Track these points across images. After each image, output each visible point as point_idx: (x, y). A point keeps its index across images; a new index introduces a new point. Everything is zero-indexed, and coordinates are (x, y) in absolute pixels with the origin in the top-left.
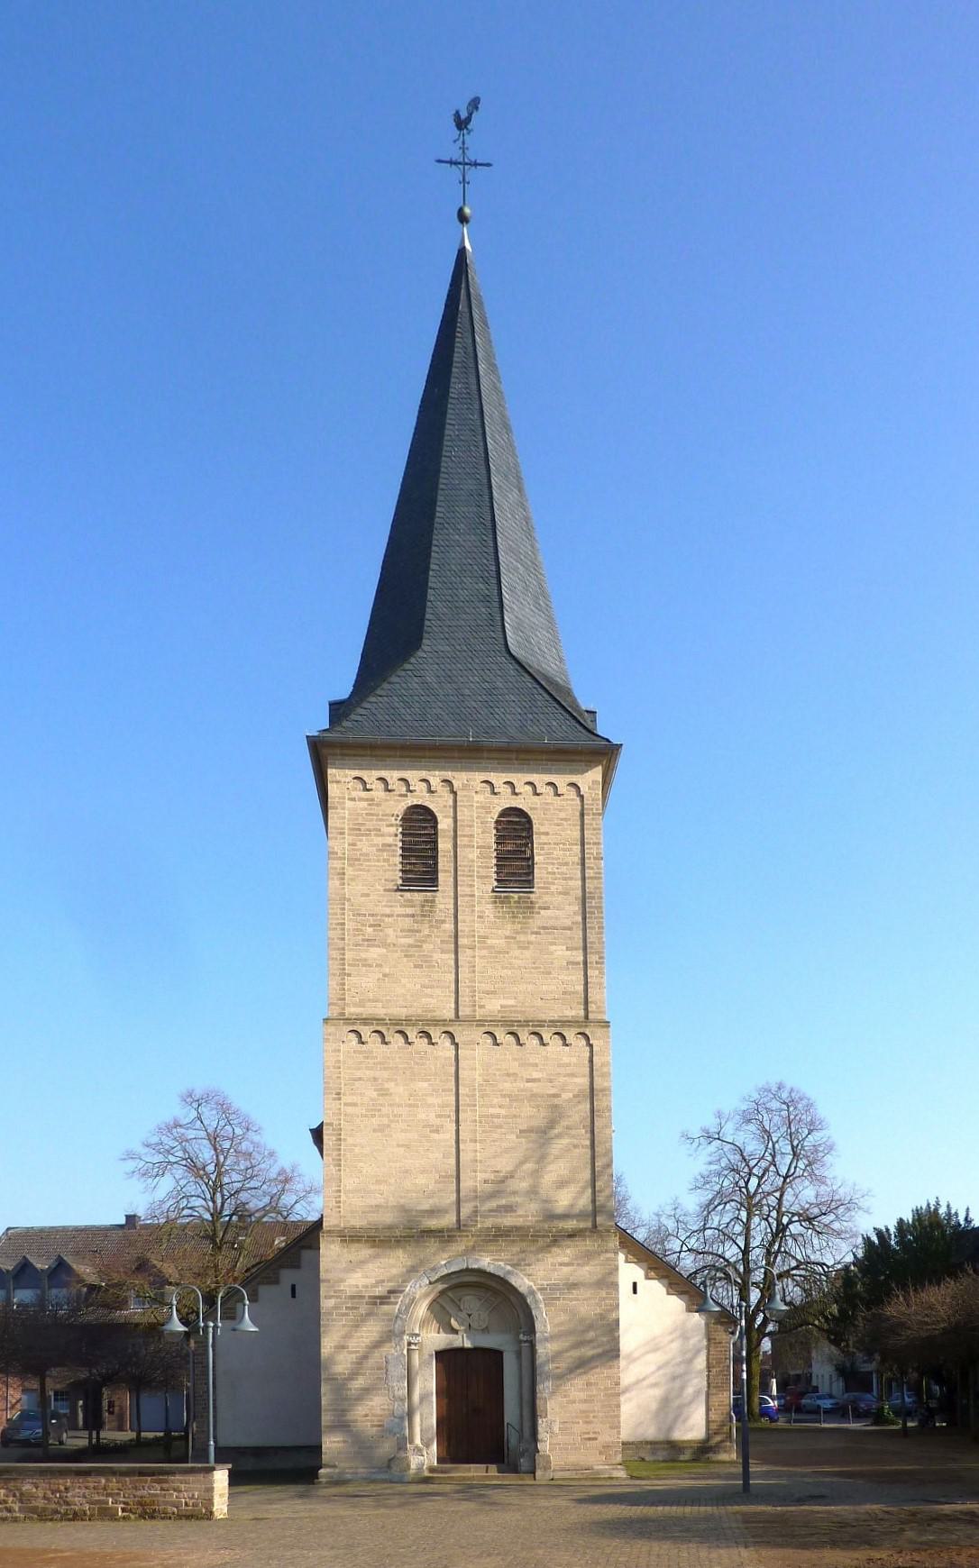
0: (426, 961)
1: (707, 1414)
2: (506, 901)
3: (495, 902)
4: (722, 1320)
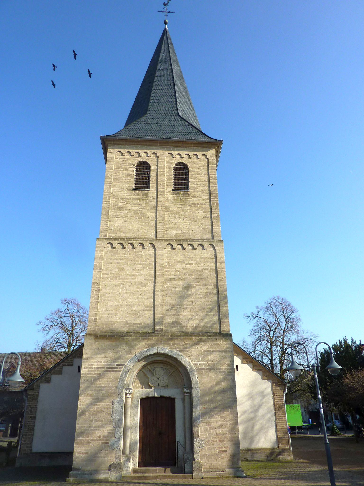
0: (144, 216)
1: (277, 434)
4: (279, 384)
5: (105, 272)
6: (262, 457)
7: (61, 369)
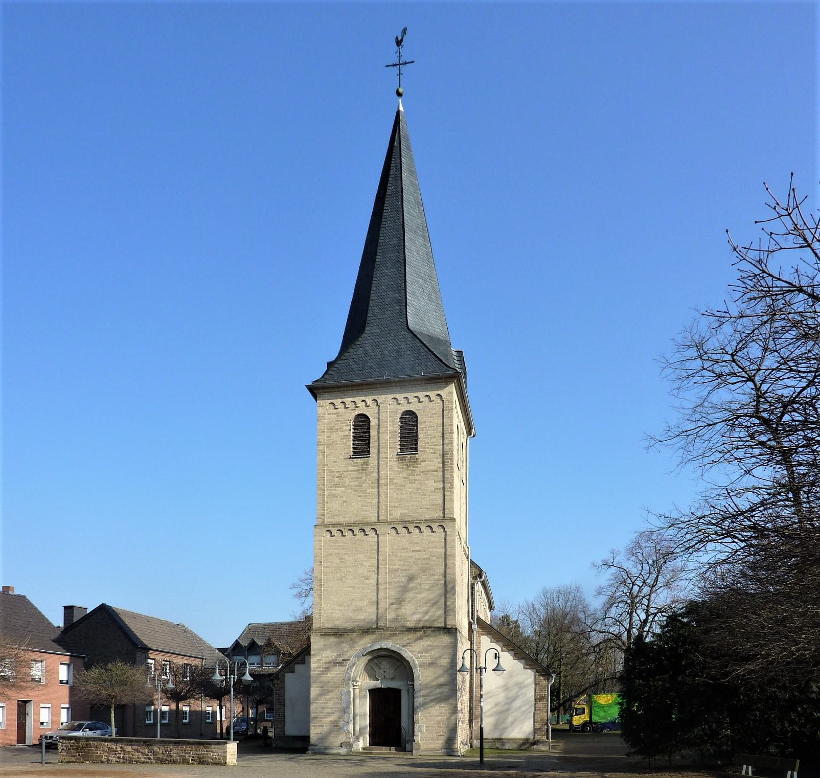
0: (364, 493)
1: (534, 725)
2: (403, 459)
3: (399, 460)
4: (543, 673)
5: (326, 565)
6: (515, 746)
7: (304, 658)
